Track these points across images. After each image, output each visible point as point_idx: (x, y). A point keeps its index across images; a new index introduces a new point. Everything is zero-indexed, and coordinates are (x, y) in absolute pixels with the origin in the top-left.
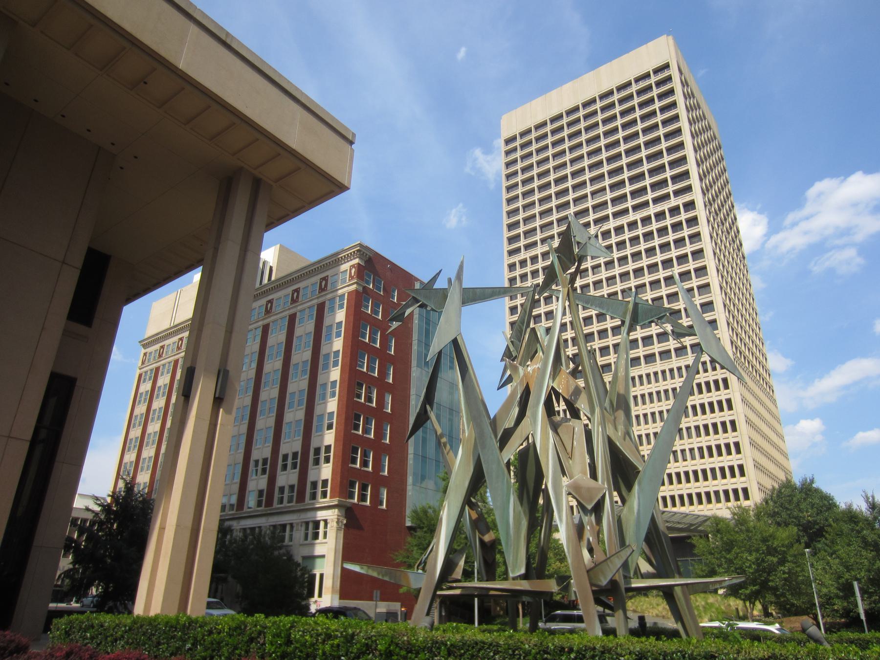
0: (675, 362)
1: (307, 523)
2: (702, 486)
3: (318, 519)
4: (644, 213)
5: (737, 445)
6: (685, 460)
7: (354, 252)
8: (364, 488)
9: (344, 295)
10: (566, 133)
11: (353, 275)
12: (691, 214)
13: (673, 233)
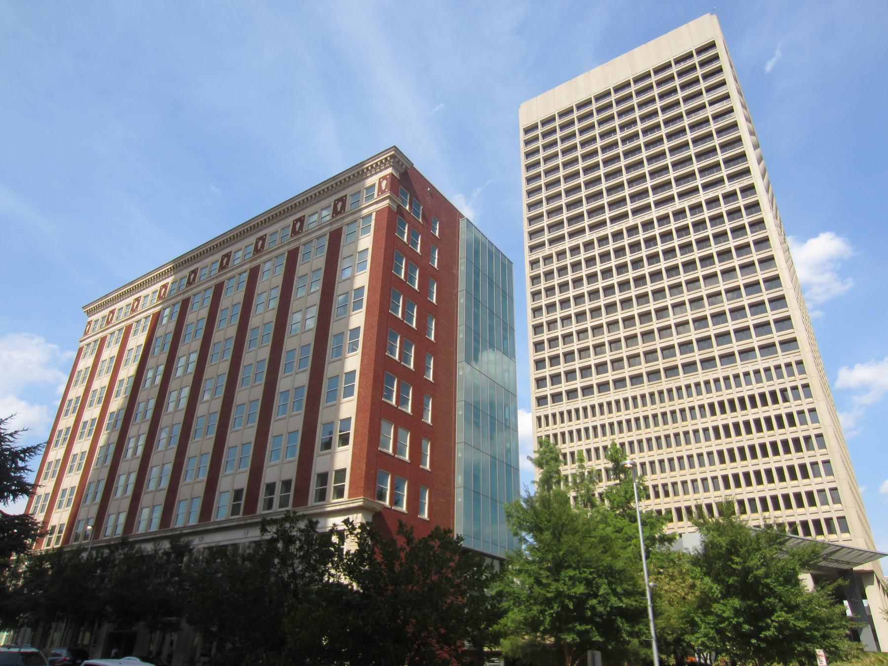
7: (386, 159)
9: (370, 215)
11: (384, 188)
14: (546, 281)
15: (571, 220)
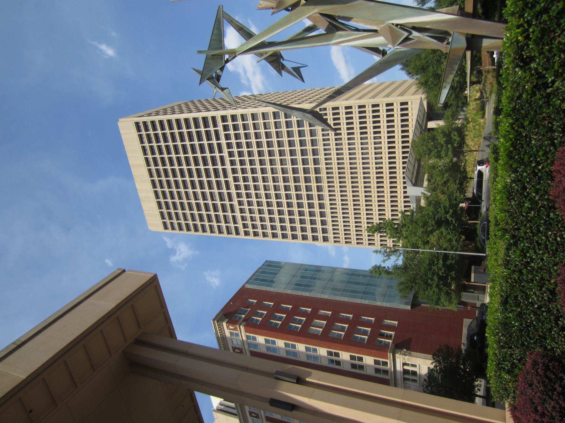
0: (319, 137)
1: (405, 379)
3: (402, 370)
4: (224, 147)
5: (373, 106)
6: (381, 153)
7: (218, 325)
8: (382, 335)
9: (247, 336)
12: (229, 119)
13: (242, 148)
14: (257, 228)
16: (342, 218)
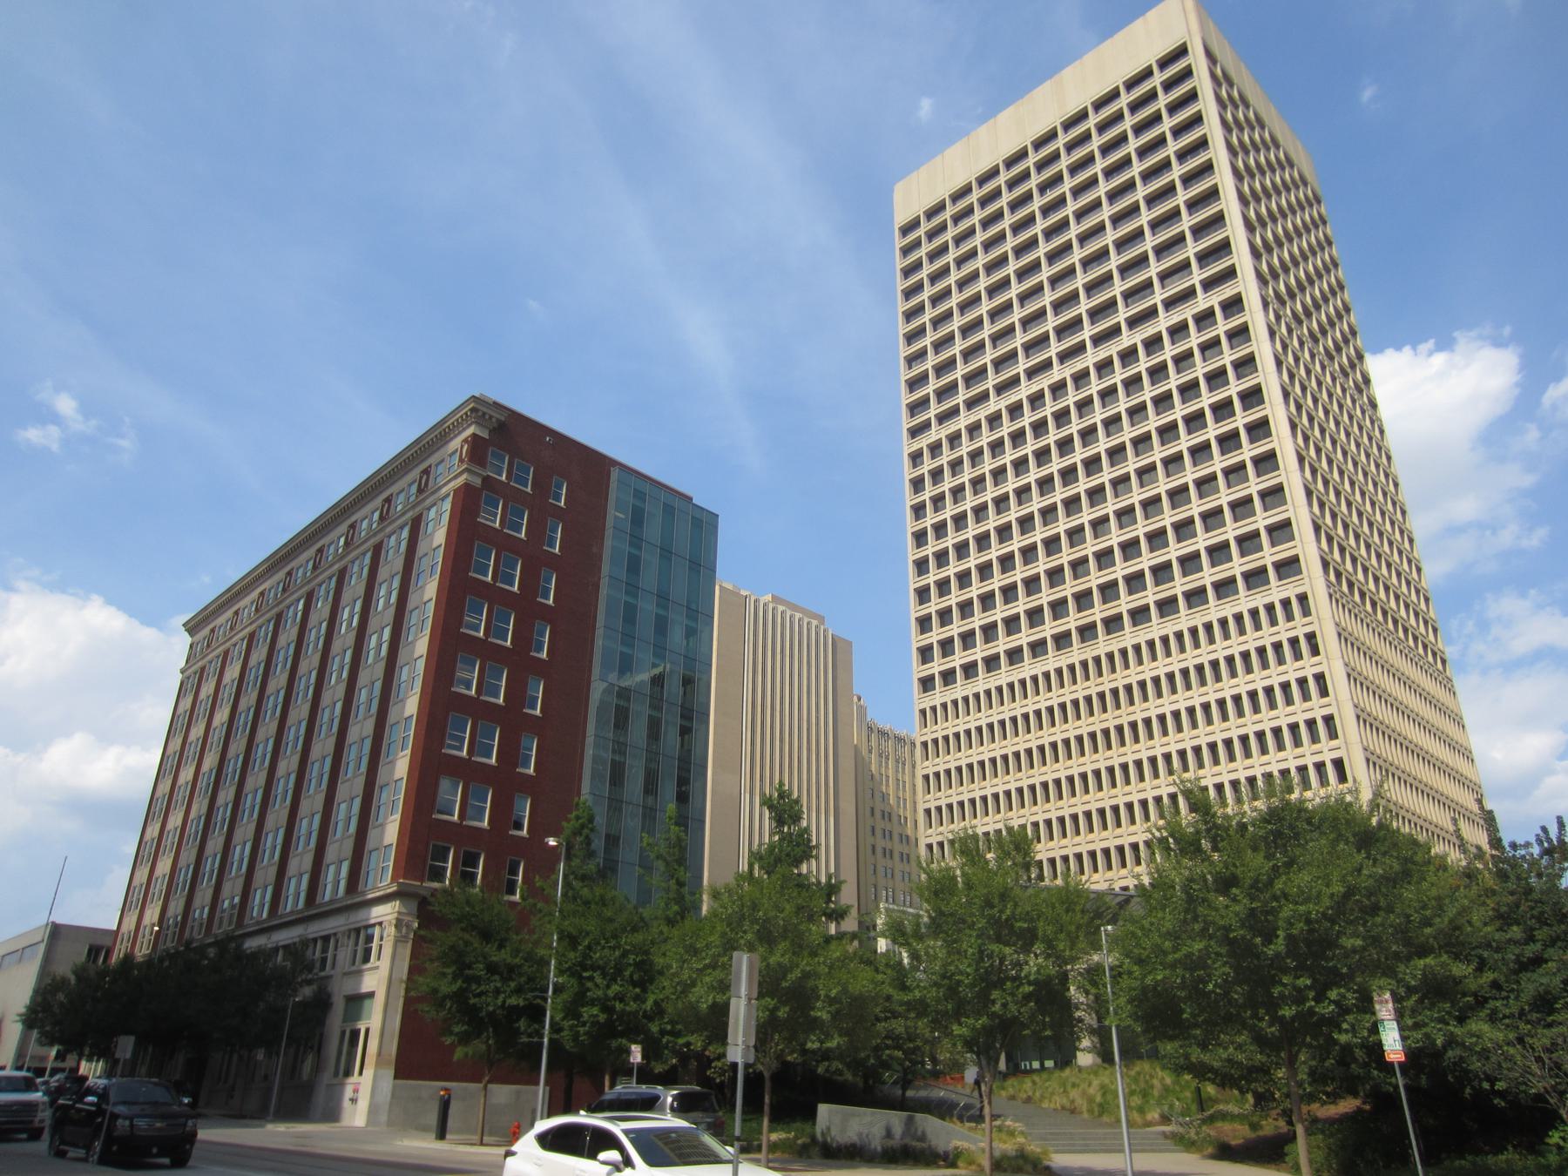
2: (978, 789)
3: (373, 921)
10: (1154, 269)
15: (1095, 314)
16: (989, 720)
